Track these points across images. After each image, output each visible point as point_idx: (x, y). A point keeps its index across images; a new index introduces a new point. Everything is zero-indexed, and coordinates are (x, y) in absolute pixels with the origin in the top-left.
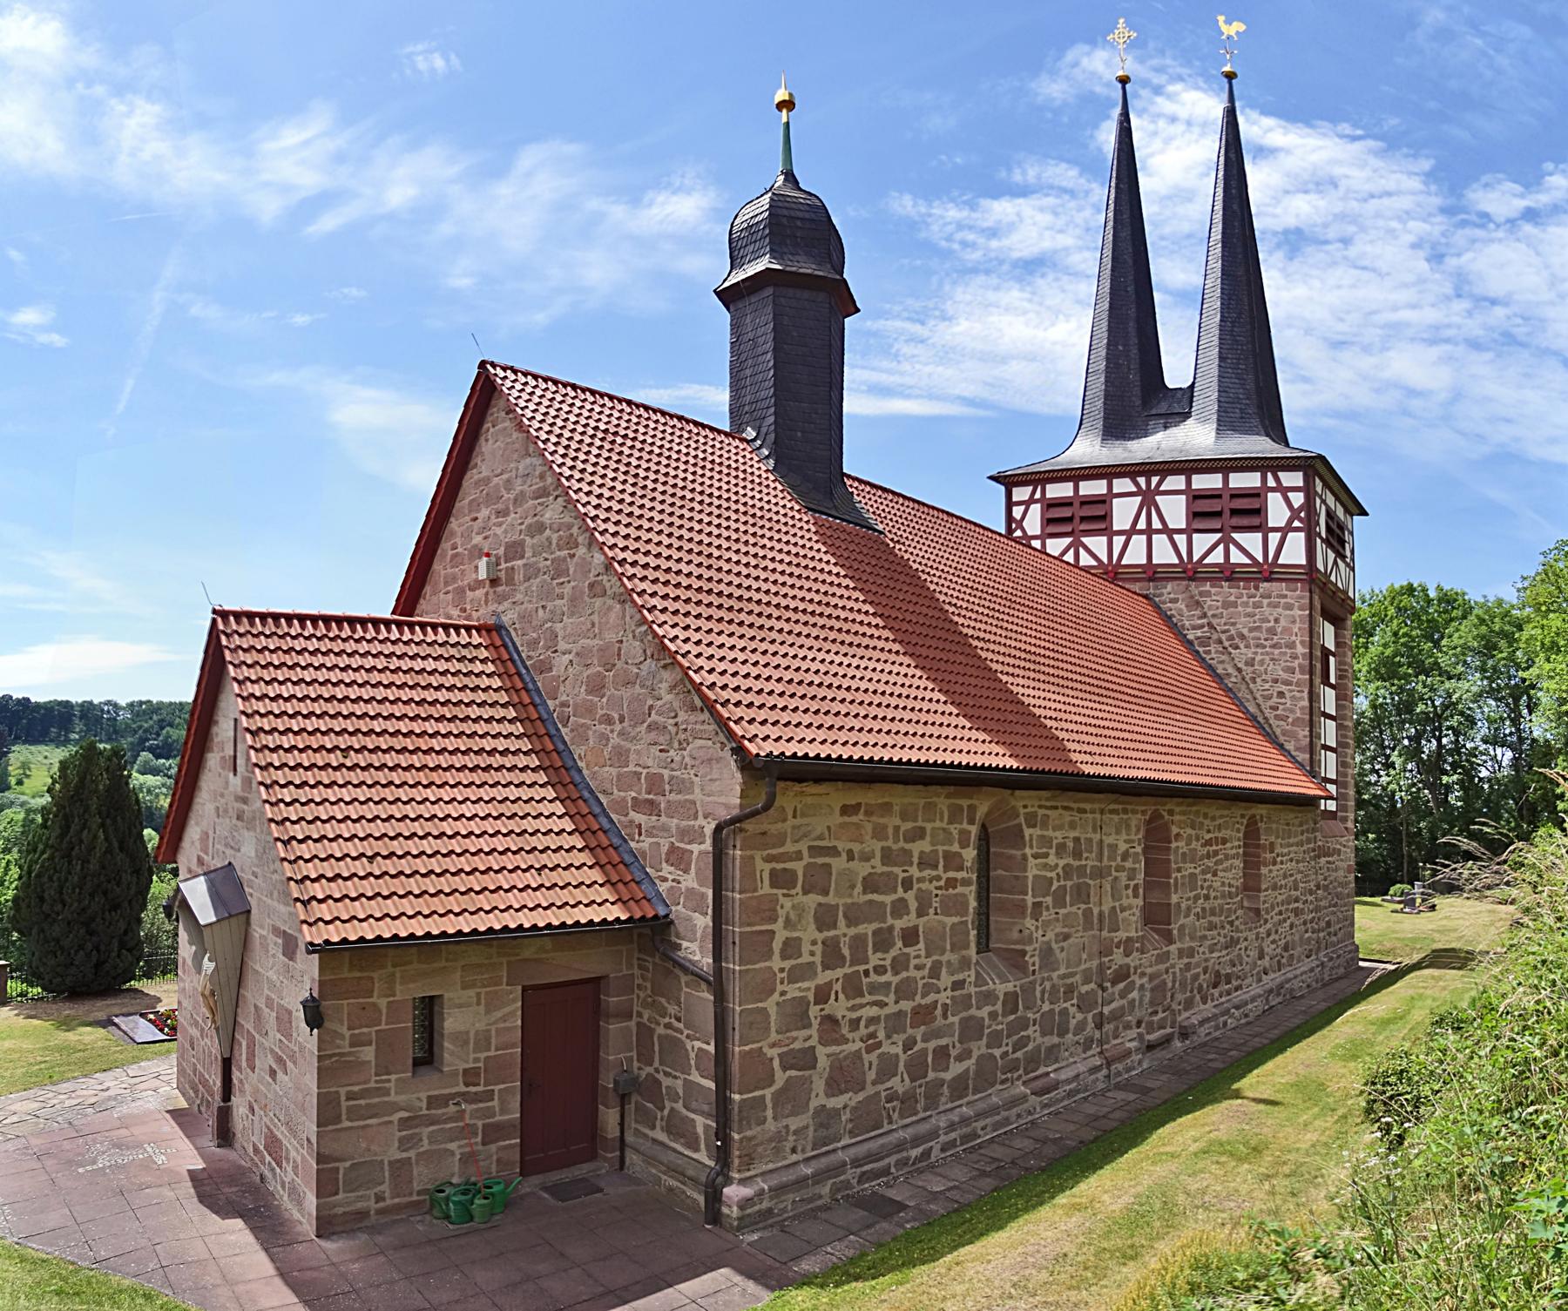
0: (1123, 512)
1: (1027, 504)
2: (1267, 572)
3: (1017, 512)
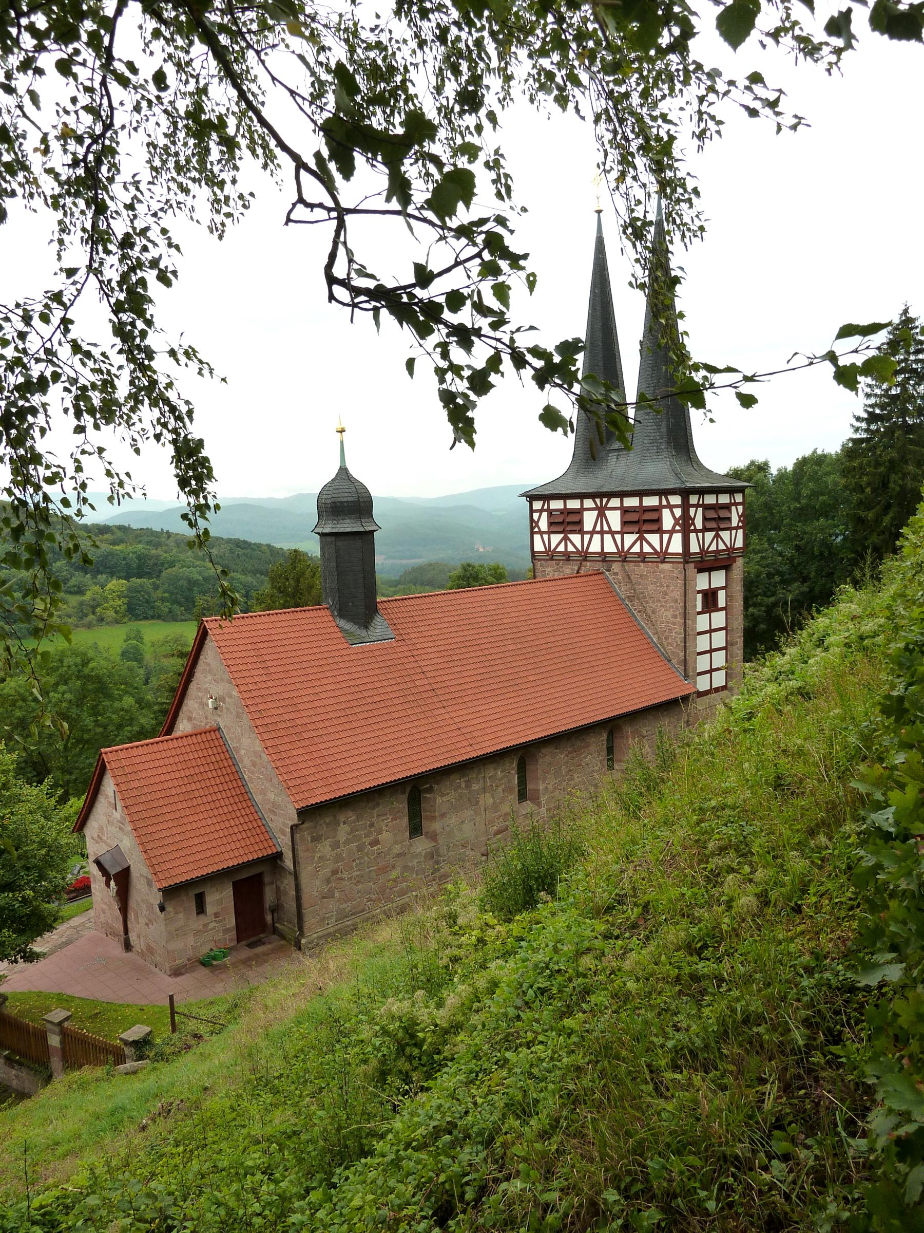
0: (589, 519)
1: (541, 511)
2: (663, 556)
3: (536, 516)
